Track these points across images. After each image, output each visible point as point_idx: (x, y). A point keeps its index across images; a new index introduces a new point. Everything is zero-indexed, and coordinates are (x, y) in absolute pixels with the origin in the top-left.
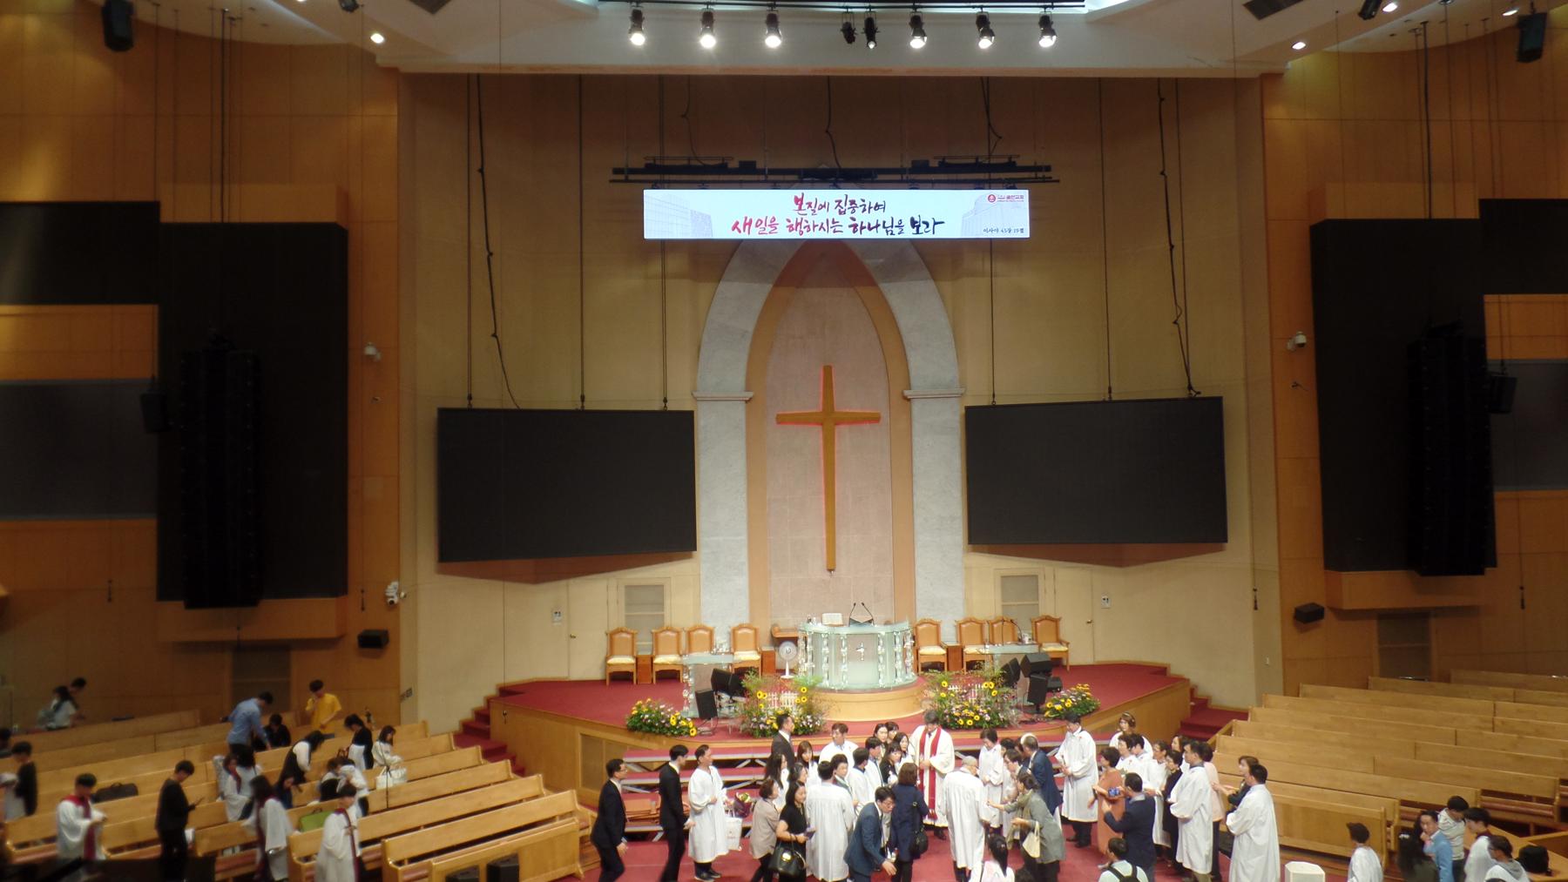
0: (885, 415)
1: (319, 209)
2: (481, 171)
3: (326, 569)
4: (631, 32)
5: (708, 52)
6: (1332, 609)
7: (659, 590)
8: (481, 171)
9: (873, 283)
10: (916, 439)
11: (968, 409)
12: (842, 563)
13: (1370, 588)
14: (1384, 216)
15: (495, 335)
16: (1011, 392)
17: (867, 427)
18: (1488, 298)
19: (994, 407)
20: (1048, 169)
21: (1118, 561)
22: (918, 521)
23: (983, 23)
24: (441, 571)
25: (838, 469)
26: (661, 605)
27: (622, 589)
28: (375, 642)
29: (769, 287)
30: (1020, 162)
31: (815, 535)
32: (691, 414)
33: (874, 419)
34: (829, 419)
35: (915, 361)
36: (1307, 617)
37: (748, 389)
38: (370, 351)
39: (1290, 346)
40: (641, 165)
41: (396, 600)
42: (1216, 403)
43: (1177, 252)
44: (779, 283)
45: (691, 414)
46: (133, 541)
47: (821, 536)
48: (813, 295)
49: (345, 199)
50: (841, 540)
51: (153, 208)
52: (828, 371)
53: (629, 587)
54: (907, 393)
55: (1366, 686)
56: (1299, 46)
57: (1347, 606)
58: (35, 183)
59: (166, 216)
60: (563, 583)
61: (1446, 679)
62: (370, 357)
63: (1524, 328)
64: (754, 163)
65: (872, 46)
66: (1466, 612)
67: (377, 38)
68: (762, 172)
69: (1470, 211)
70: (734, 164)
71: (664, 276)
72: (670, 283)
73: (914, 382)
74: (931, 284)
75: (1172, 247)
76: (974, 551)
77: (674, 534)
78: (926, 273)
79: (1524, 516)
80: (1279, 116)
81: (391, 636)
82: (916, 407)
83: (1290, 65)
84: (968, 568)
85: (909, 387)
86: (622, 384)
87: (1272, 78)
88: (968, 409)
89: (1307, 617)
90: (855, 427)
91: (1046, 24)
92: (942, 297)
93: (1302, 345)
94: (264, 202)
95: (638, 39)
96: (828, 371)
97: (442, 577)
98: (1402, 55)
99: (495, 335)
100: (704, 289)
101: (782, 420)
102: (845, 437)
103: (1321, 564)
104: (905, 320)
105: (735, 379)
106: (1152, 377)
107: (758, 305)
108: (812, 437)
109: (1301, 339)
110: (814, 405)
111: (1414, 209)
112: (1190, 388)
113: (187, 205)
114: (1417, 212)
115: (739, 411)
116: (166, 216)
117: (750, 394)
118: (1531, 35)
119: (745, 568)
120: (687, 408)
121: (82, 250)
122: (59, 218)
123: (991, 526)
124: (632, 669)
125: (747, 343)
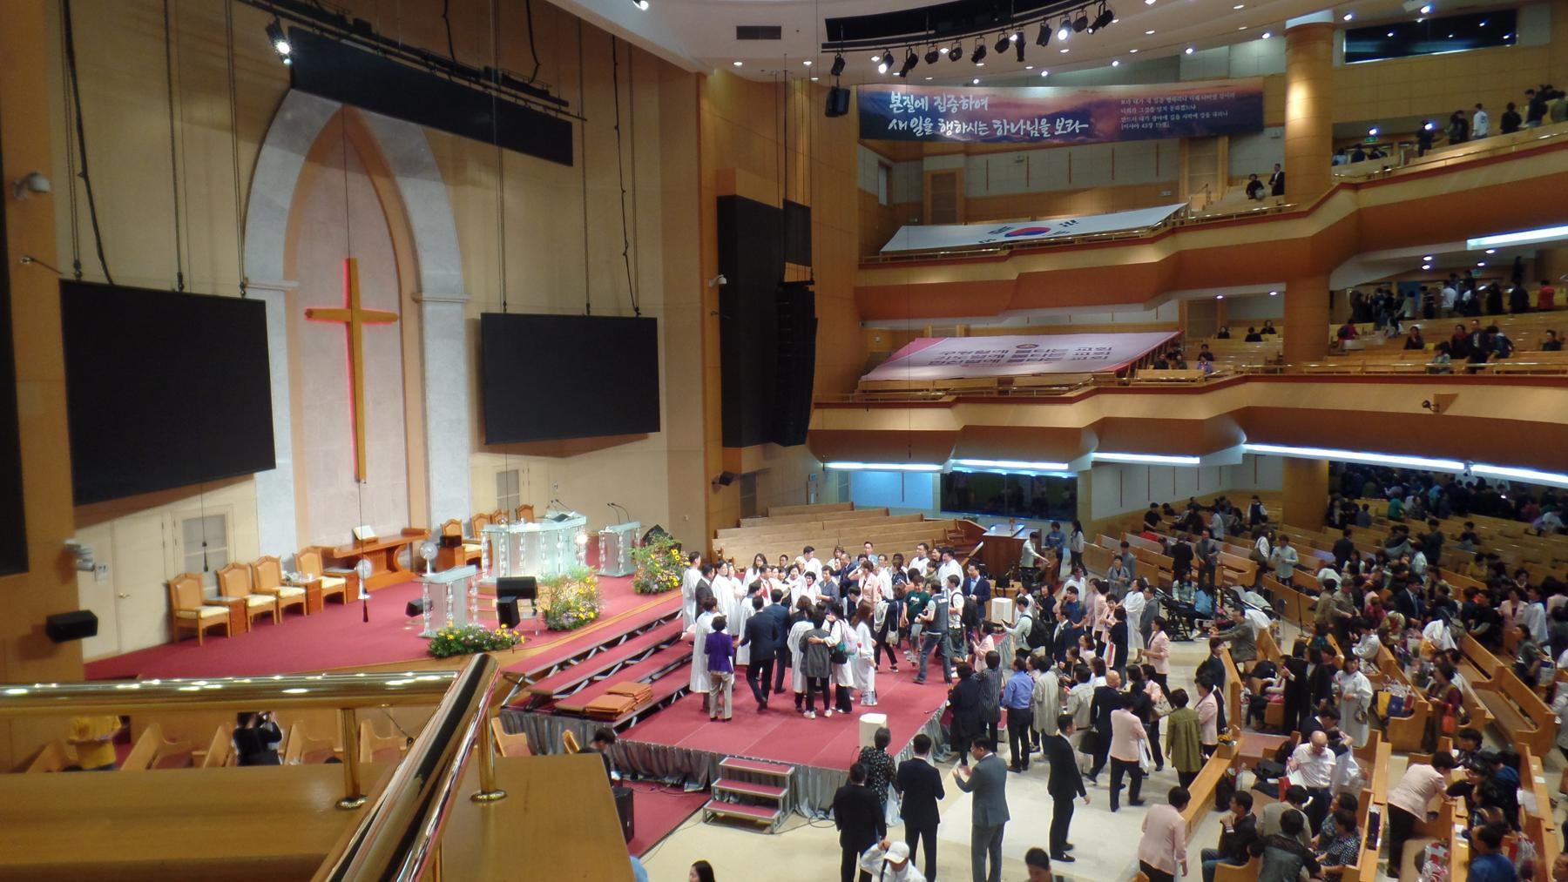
7: (222, 520)
12: (370, 471)
14: (751, 197)
16: (524, 302)
17: (381, 327)
21: (561, 453)
26: (223, 539)
27: (180, 525)
30: (553, 93)
36: (725, 479)
42: (654, 321)
43: (628, 198)
53: (188, 523)
55: (738, 526)
61: (766, 515)
67: (808, 63)
68: (376, 37)
96: (350, 265)
103: (720, 443)
104: (419, 221)
106: (608, 303)
107: (293, 179)
110: (338, 302)
119: (292, 487)
124: (303, 600)
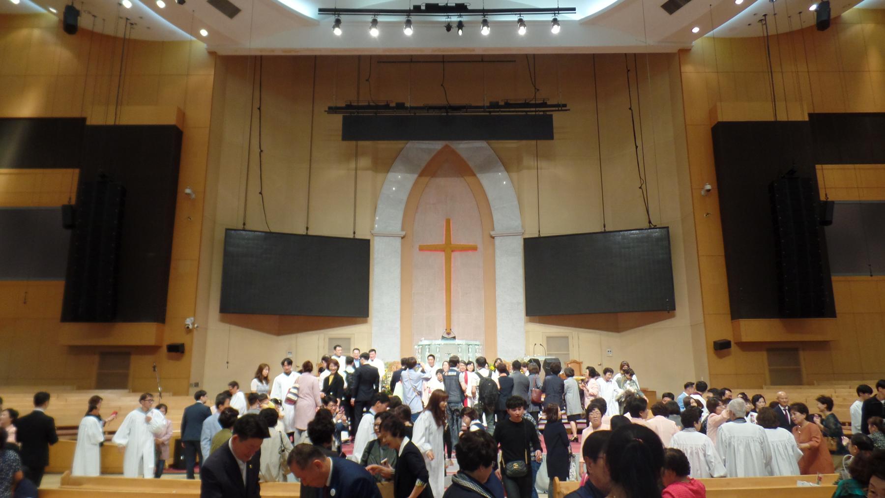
0: (480, 247)
1: (169, 119)
2: (259, 109)
3: (153, 305)
4: (334, 27)
5: (375, 39)
6: (736, 343)
8: (259, 109)
9: (474, 175)
10: (497, 259)
11: (525, 240)
13: (755, 329)
15: (261, 193)
16: (549, 230)
17: (470, 253)
18: (818, 167)
19: (539, 238)
20: (565, 106)
21: (616, 328)
22: (498, 305)
23: (521, 21)
24: (223, 320)
25: (453, 276)
27: (327, 340)
28: (177, 350)
29: (416, 176)
31: (440, 312)
32: (368, 241)
33: (474, 249)
34: (448, 249)
35: (496, 217)
37: (403, 229)
38: (188, 191)
39: (703, 193)
40: (344, 105)
41: (191, 327)
43: (640, 148)
44: (421, 175)
45: (368, 241)
46: (51, 292)
47: (444, 314)
48: (441, 181)
49: (182, 115)
50: (455, 316)
51: (84, 120)
52: (448, 222)
53: (330, 339)
54: (492, 233)
56: (696, 30)
57: (745, 339)
58: (27, 107)
59: (88, 123)
60: (294, 336)
62: (188, 194)
63: (840, 183)
64: (403, 104)
65: (460, 32)
66: (822, 346)
69: (807, 119)
70: (393, 105)
71: (356, 169)
72: (359, 172)
73: (496, 228)
74: (505, 174)
75: (637, 147)
76: (531, 321)
77: (355, 307)
78: (502, 168)
79: (847, 289)
80: (689, 71)
81: (187, 348)
82: (497, 241)
83: (694, 43)
84: (527, 332)
85: (493, 229)
86: (332, 224)
87: (685, 52)
88: (525, 240)
89: (721, 347)
90: (464, 254)
91: (555, 21)
92: (512, 182)
93: (709, 191)
94: (139, 114)
95: (338, 32)
96: (448, 222)
97: (226, 327)
98: (759, 38)
99: (261, 193)
100: (380, 176)
101: (422, 249)
102: (456, 255)
105: (396, 226)
106: (626, 219)
108: (441, 257)
109: (708, 187)
111: (766, 116)
112: (650, 222)
113: (97, 117)
114: (769, 117)
115: (397, 243)
116: (88, 123)
117: (403, 233)
118: (825, 22)
119: (398, 332)
120: (368, 238)
121: (47, 141)
122: (41, 128)
123: (541, 305)
125: (403, 206)
